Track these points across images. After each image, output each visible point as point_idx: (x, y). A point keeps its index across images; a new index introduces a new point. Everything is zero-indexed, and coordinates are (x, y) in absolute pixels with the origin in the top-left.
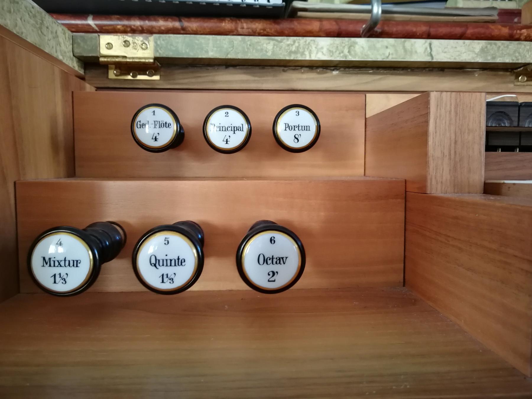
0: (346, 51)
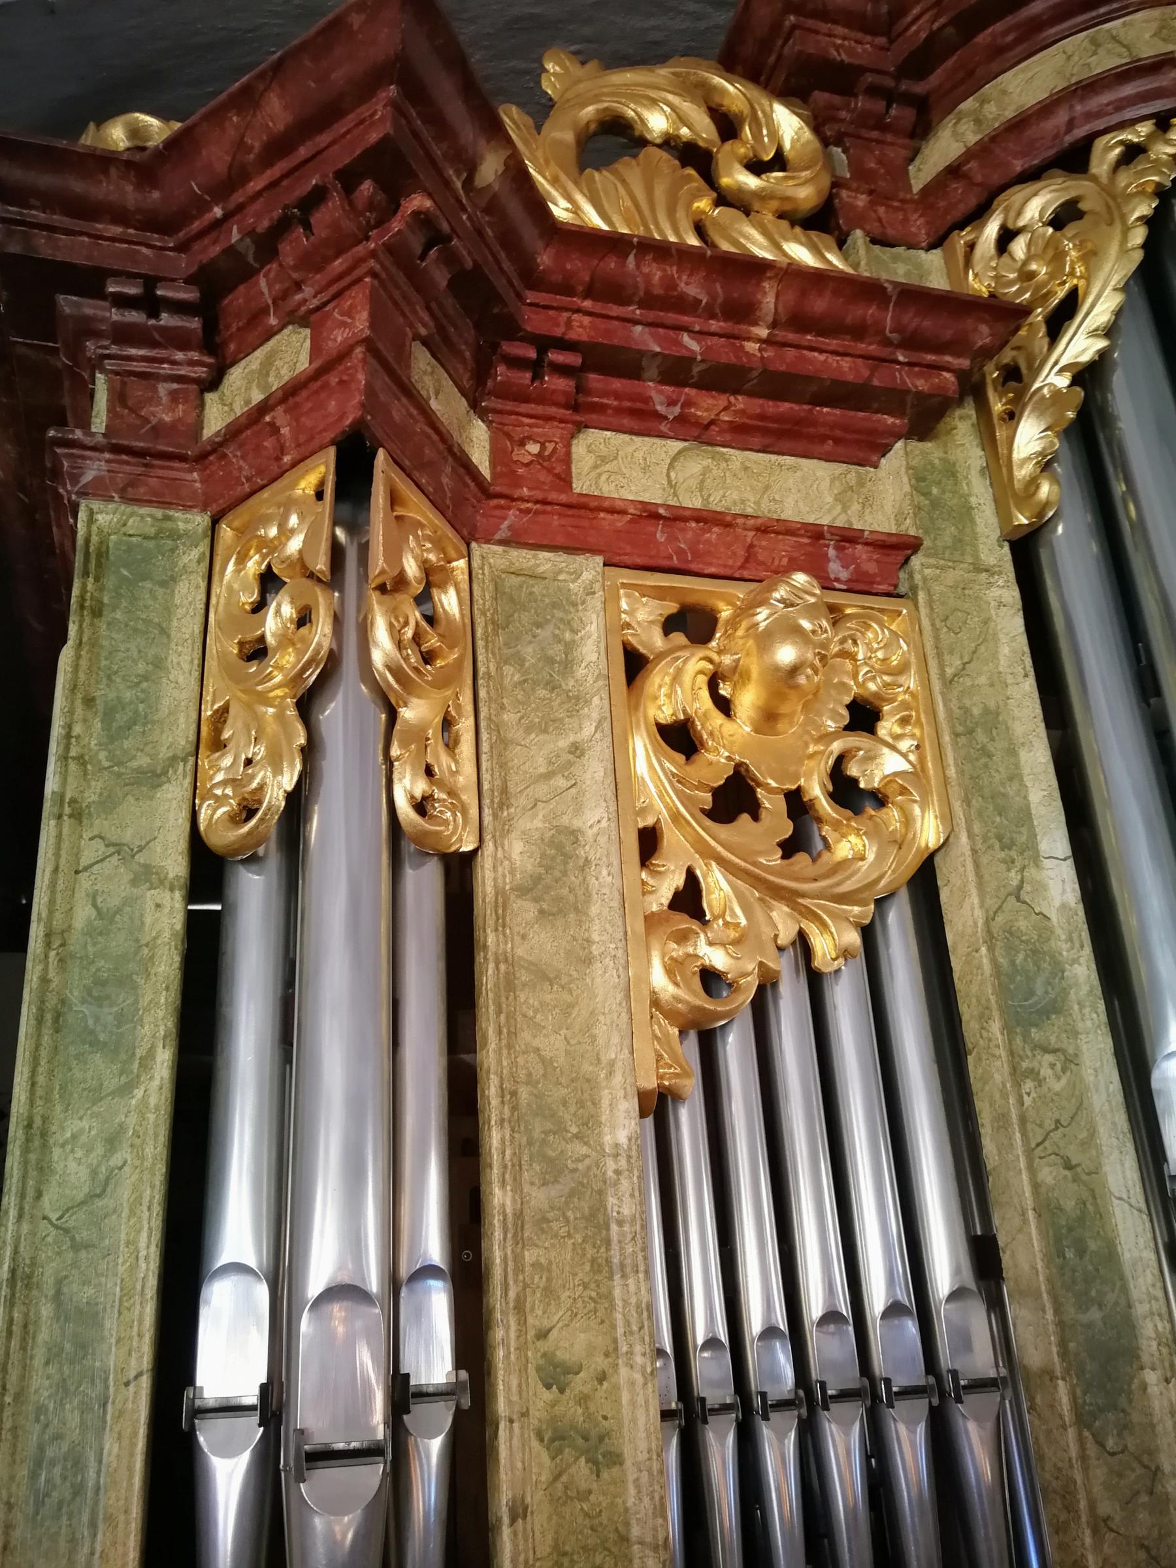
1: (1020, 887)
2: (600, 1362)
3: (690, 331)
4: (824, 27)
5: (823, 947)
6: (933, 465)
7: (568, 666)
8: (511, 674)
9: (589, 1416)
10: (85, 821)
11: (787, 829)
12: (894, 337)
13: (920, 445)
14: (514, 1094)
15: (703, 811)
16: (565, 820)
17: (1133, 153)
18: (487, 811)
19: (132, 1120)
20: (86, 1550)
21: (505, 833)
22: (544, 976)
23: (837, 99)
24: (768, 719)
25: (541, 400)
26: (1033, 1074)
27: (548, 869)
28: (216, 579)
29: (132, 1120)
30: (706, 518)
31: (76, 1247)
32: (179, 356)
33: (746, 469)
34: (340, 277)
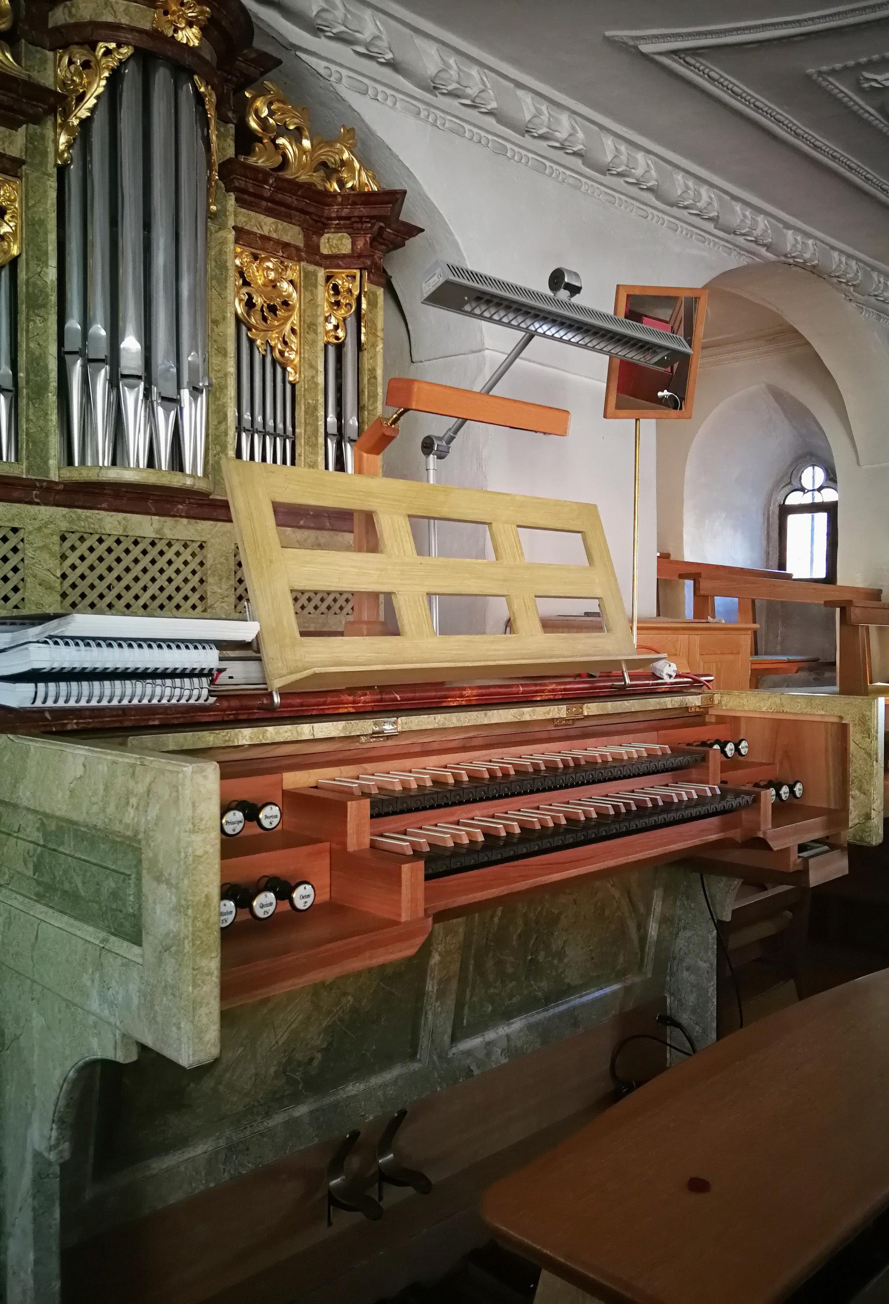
0: (261, 737)
1: (40, 272)
17: (108, 52)
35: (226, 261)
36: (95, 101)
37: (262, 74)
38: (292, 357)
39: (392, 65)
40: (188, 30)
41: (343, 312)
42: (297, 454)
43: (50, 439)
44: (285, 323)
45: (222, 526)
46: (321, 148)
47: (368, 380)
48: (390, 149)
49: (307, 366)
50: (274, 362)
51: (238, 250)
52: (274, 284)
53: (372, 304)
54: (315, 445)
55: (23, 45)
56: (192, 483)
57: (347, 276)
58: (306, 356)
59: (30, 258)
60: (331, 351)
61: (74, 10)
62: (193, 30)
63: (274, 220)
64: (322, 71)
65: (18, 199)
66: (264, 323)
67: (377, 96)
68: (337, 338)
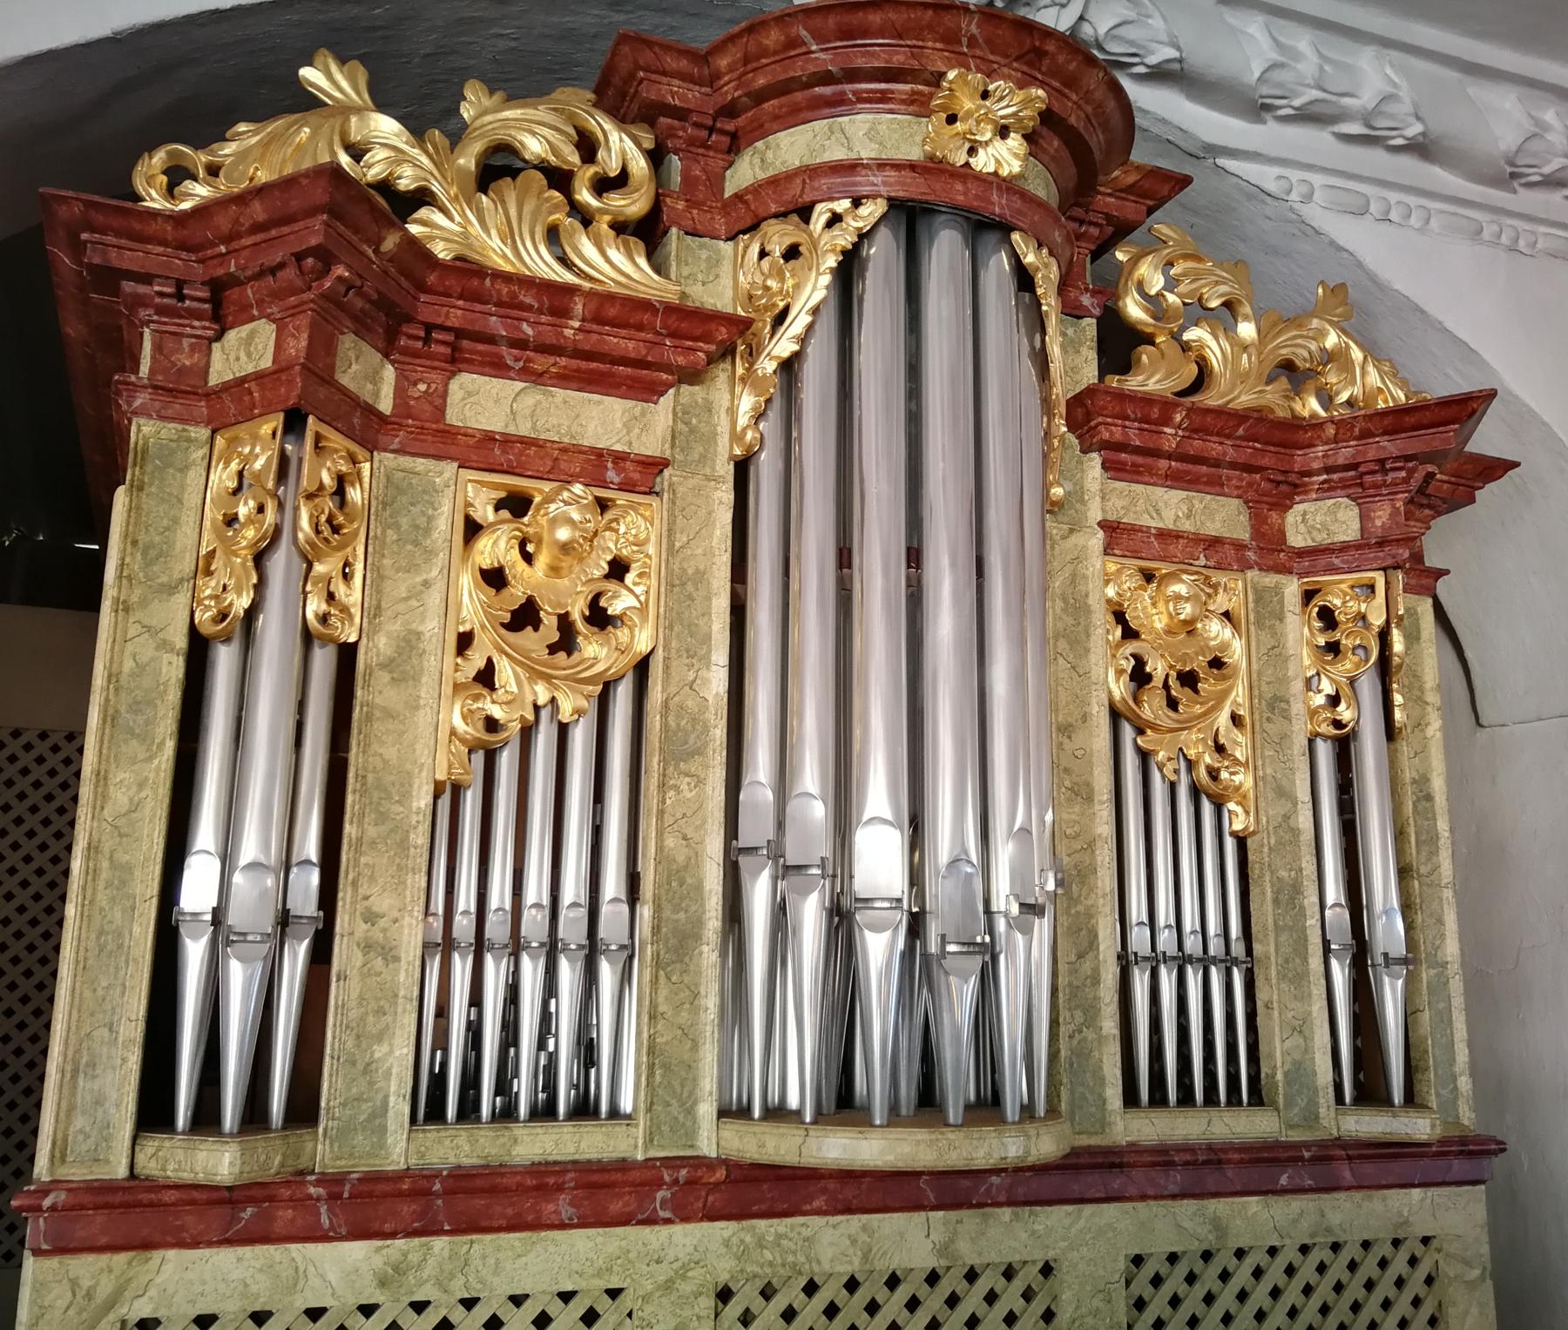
1: (694, 681)
2: (395, 914)
3: (527, 321)
4: (665, 80)
5: (566, 712)
6: (696, 402)
7: (427, 531)
8: (391, 535)
9: (385, 937)
10: (131, 613)
11: (555, 637)
12: (663, 331)
13: (690, 388)
14: (364, 777)
15: (503, 625)
16: (414, 626)
17: (835, 219)
18: (365, 620)
19: (152, 775)
20: (123, 973)
21: (375, 632)
22: (390, 714)
23: (676, 123)
24: (554, 570)
25: (430, 356)
26: (676, 788)
27: (400, 654)
28: (212, 470)
29: (152, 775)
30: (527, 442)
31: (121, 835)
32: (196, 323)
33: (565, 402)
34: (294, 307)
35: (1087, 595)
36: (809, 319)
37: (1150, 211)
38: (1237, 779)
39: (1421, 148)
40: (998, 143)
41: (1348, 666)
42: (1259, 1004)
43: (701, 1053)
44: (1217, 707)
45: (1093, 1215)
46: (1279, 334)
47: (1414, 804)
48: (1423, 312)
49: (1271, 795)
50: (1196, 792)
51: (1112, 567)
52: (1189, 627)
53: (1412, 638)
54: (1299, 978)
55: (674, 238)
56: (1021, 1153)
57: (1352, 587)
58: (1269, 771)
59: (673, 655)
60: (1324, 752)
61: (770, 155)
62: (1010, 142)
63: (1185, 494)
64: (1271, 186)
65: (653, 538)
66: (1172, 714)
67: (1388, 212)
68: (1338, 724)
